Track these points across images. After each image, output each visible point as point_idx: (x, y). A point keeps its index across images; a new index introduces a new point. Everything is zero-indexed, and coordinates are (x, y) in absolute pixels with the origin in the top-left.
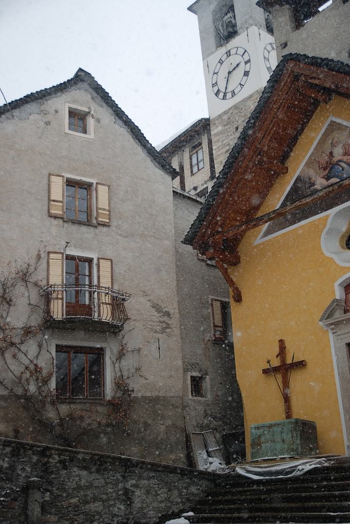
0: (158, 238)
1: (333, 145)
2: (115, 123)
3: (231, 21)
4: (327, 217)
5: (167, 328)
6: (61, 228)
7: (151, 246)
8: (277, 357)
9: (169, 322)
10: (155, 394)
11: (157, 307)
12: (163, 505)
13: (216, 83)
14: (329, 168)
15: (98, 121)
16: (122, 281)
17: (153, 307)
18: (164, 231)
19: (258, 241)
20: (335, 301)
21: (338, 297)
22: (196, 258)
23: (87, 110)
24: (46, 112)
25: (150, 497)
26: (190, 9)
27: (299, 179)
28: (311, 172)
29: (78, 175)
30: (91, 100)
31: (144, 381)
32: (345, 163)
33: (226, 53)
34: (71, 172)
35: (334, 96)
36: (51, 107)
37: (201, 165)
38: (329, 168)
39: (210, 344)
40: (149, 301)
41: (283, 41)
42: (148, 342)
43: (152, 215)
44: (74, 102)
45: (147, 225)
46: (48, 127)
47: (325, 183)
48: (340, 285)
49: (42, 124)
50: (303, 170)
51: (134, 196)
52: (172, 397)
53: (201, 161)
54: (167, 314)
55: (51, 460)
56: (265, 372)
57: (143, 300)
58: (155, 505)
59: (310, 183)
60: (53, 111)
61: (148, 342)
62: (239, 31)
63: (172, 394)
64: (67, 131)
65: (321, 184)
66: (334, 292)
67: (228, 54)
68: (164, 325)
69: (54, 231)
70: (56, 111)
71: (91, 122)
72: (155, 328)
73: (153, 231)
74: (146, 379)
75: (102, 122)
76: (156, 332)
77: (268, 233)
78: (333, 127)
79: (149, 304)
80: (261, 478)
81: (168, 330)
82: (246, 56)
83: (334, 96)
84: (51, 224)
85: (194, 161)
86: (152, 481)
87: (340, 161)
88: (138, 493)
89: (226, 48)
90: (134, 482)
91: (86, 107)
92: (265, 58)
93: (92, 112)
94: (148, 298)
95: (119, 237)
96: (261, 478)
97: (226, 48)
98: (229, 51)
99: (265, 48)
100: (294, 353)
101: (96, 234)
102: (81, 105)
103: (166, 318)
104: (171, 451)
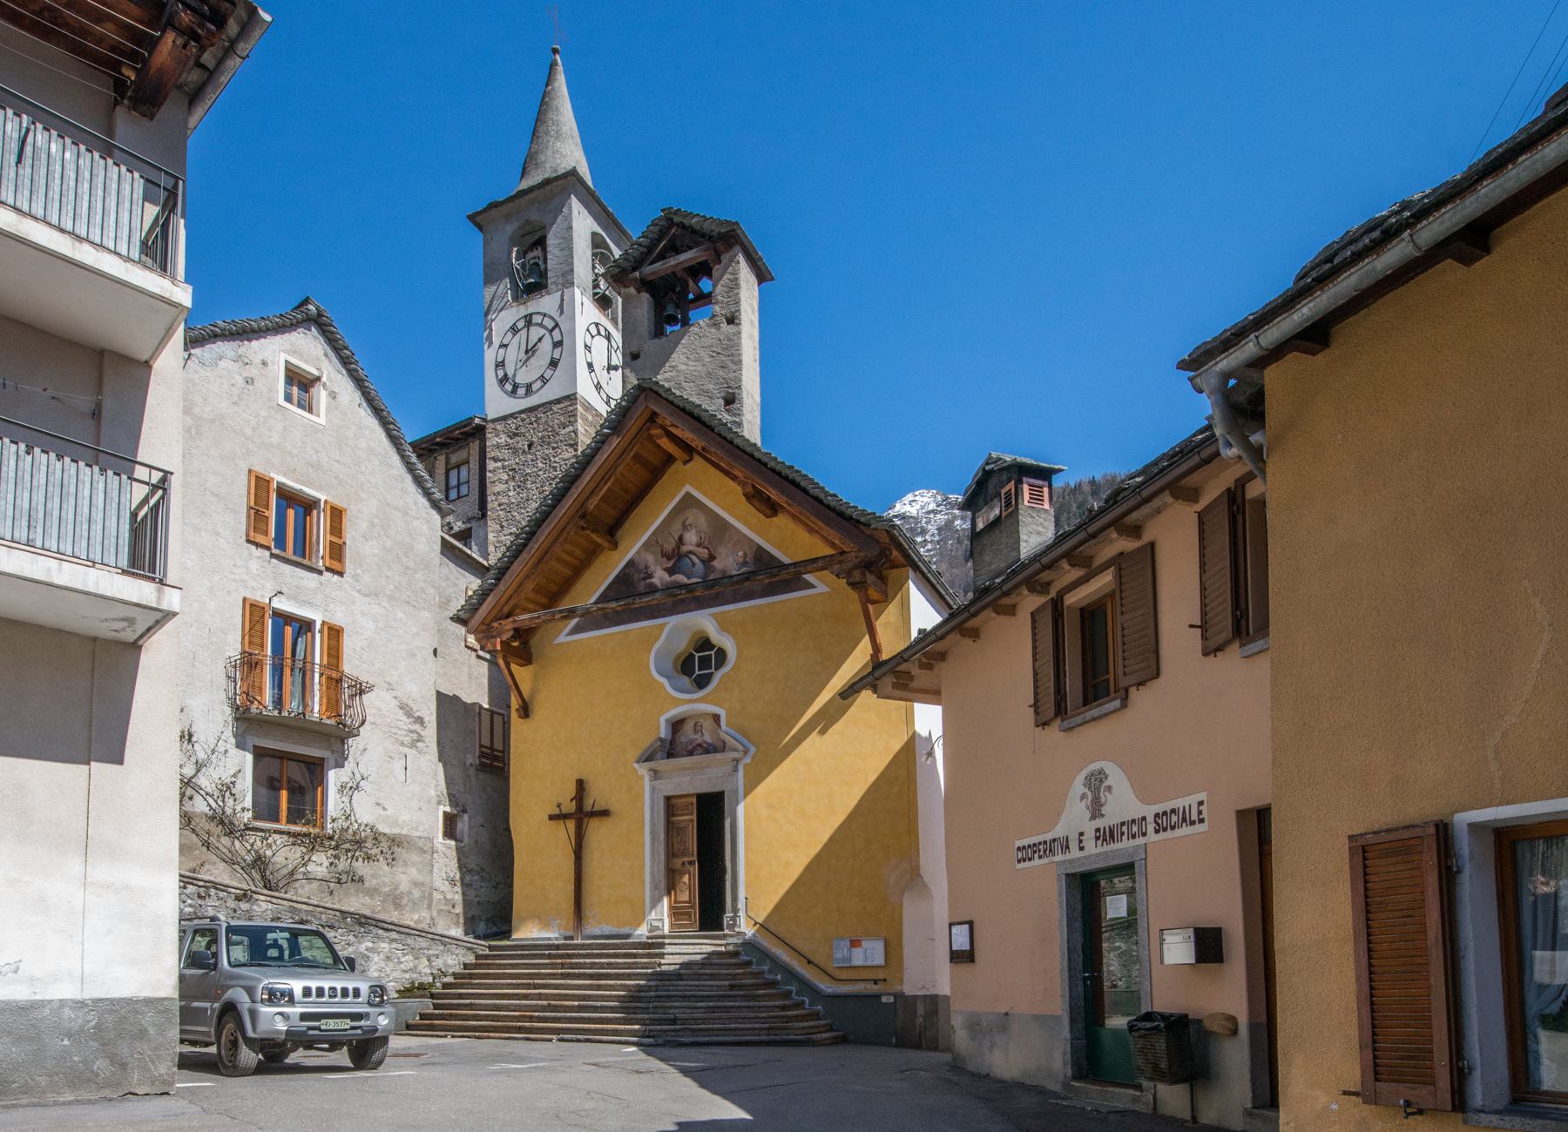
0: (414, 606)
1: (685, 527)
2: (359, 405)
3: (537, 264)
4: (665, 624)
5: (418, 741)
6: (266, 564)
7: (403, 616)
8: (572, 800)
9: (423, 733)
10: (396, 831)
11: (405, 708)
12: (407, 976)
13: (503, 362)
14: (676, 558)
15: (333, 396)
16: (357, 663)
17: (401, 708)
18: (423, 595)
19: (562, 638)
20: (661, 740)
21: (663, 735)
22: (463, 644)
23: (316, 373)
24: (247, 361)
25: (391, 965)
26: (472, 218)
27: (631, 563)
28: (650, 558)
29: (297, 481)
30: (324, 358)
31: (382, 812)
32: (698, 557)
33: (526, 317)
34: (285, 475)
35: (697, 458)
36: (255, 353)
37: (464, 490)
38: (676, 558)
39: (472, 771)
40: (395, 698)
41: (634, 349)
42: (391, 757)
43: (408, 568)
44: (293, 352)
45: (399, 582)
46: (250, 387)
47: (667, 577)
48: (667, 721)
49: (240, 381)
50: (638, 552)
51: (382, 533)
52: (420, 837)
53: (454, 487)
54: (420, 721)
55: (255, 907)
56: (551, 818)
57: (387, 696)
58: (397, 974)
59: (646, 573)
60: (259, 362)
61: (391, 757)
62: (550, 287)
63: (419, 834)
64: (282, 402)
65: (661, 579)
66: (658, 727)
67: (528, 320)
68: (415, 736)
69: (254, 566)
70: (264, 363)
71: (321, 396)
72: (401, 738)
73: (408, 593)
74: (385, 809)
75: (340, 398)
76: (402, 744)
77: (576, 630)
78: (689, 502)
79: (395, 703)
80: (1204, 435)
81: (419, 744)
82: (556, 333)
83: (697, 458)
84: (250, 555)
85: (453, 482)
86: (394, 945)
87: (691, 552)
88: (376, 958)
89: (527, 309)
90: (370, 945)
91: (314, 366)
92: (586, 346)
93: (324, 379)
94: (394, 693)
95: (356, 594)
96: (1204, 435)
97: (527, 309)
98: (531, 315)
99: (588, 330)
100: (595, 799)
101: (321, 584)
102: (306, 362)
103: (417, 727)
104: (413, 910)
